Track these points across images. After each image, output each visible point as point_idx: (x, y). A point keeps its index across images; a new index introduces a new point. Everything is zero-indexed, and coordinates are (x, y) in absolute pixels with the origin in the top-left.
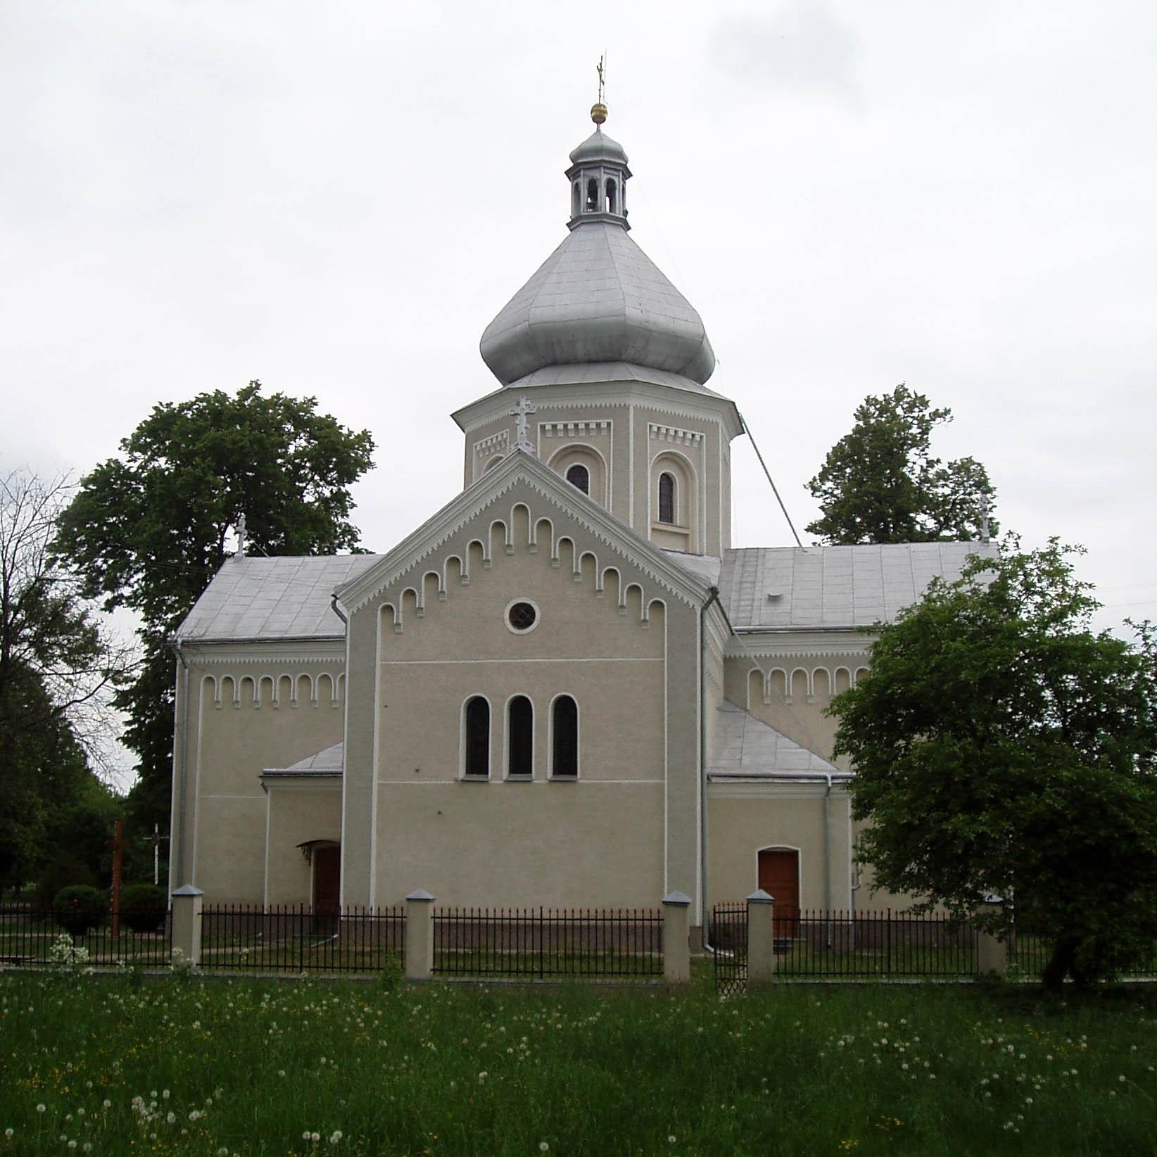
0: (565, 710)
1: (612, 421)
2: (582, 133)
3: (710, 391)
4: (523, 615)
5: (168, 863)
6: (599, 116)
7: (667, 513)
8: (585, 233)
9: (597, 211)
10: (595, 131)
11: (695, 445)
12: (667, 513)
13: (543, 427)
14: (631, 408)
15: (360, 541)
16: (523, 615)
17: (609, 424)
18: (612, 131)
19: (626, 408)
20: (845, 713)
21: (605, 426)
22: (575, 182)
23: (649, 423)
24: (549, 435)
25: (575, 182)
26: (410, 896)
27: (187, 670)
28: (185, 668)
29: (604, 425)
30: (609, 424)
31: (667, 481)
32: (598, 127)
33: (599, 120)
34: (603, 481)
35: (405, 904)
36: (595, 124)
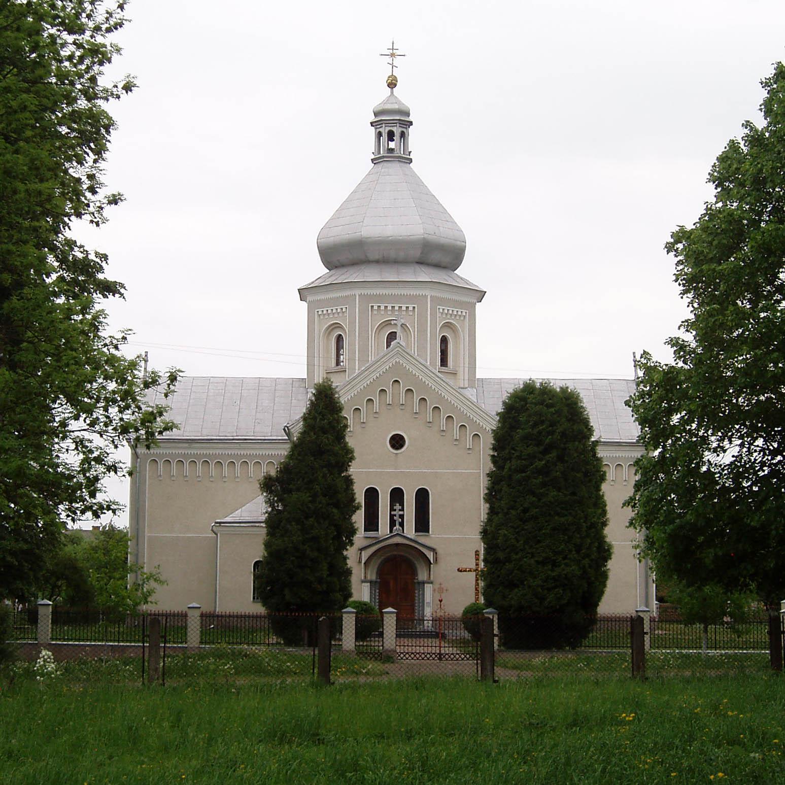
0: (422, 496)
1: (416, 306)
2: (379, 96)
3: (466, 282)
4: (397, 442)
5: (656, 595)
6: (392, 84)
7: (444, 362)
8: (385, 168)
9: (392, 153)
10: (390, 94)
11: (462, 318)
12: (444, 362)
13: (372, 307)
14: (429, 297)
15: (622, 507)
16: (397, 442)
17: (414, 308)
18: (404, 96)
19: (426, 296)
20: (669, 528)
21: (412, 309)
22: (378, 130)
23: (438, 307)
24: (375, 312)
25: (378, 130)
26: (189, 606)
27: (139, 460)
28: (138, 458)
29: (411, 309)
30: (414, 308)
31: (444, 340)
32: (392, 93)
33: (392, 86)
34: (406, 342)
35: (187, 610)
36: (390, 89)
